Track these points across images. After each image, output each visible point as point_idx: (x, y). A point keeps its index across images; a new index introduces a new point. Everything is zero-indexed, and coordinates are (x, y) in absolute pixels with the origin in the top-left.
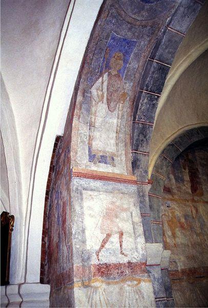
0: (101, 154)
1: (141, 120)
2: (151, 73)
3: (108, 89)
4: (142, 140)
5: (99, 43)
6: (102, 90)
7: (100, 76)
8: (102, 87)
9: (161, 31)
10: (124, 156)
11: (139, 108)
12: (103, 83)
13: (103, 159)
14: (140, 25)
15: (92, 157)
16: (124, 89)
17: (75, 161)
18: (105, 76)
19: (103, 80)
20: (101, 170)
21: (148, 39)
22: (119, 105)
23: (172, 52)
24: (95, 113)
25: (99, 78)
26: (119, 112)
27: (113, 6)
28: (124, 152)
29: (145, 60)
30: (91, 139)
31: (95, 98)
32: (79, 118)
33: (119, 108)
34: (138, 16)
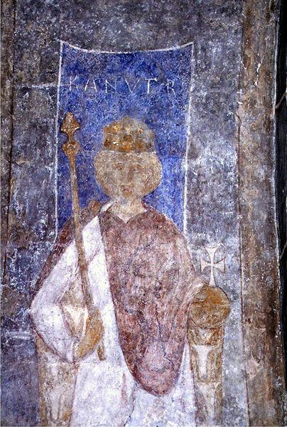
6: (87, 300)
7: (64, 240)
12: (83, 267)
16: (198, 272)
18: (91, 234)
19: (81, 253)
21: (235, 24)
22: (194, 353)
25: (60, 251)
26: (204, 388)
29: (259, 120)
31: (59, 346)
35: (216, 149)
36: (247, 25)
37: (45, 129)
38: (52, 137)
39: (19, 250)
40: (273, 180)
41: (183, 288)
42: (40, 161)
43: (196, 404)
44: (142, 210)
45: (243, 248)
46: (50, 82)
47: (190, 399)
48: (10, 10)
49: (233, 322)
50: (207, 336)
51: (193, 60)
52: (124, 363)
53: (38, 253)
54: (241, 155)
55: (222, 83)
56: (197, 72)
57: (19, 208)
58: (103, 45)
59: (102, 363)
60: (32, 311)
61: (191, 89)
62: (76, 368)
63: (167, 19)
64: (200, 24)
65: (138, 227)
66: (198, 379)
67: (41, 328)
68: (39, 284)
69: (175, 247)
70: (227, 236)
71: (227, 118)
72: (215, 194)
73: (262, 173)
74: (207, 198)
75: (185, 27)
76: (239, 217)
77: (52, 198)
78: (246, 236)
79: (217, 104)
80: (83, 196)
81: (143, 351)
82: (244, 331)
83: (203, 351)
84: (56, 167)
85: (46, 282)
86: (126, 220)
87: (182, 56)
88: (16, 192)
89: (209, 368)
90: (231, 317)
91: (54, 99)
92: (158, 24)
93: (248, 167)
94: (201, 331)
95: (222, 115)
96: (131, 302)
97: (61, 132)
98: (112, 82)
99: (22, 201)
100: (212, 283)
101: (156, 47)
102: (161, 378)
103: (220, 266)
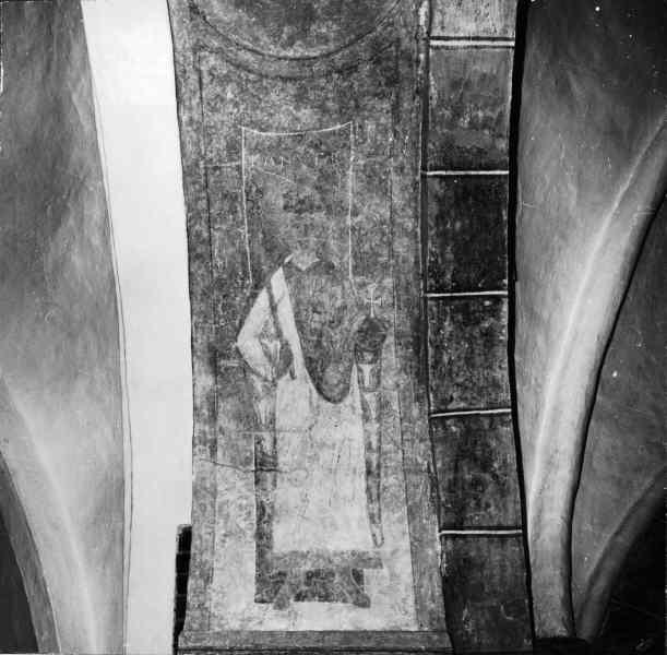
0: (308, 567)
1: (450, 407)
2: (432, 224)
3: (300, 325)
4: (477, 483)
5: (212, 180)
6: (279, 334)
7: (257, 287)
8: (276, 323)
9: (418, 61)
10: (407, 558)
11: (431, 361)
12: (273, 308)
13: (318, 585)
14: (329, 74)
15: (273, 584)
16: (362, 307)
17: (201, 606)
18: (278, 280)
19: (271, 298)
20: (304, 625)
21: (386, 105)
22: (360, 370)
23: (487, 119)
24: (273, 421)
25: (254, 296)
26: (368, 396)
27: (203, 47)
28: (405, 544)
29: (408, 181)
30: (264, 514)
31: (262, 371)
32: (213, 451)
33: (361, 381)
34: (309, 45)
35: (373, 207)
36: (396, 108)
37: (235, 198)
38: (241, 205)
39: (224, 297)
40: (419, 230)
41: (351, 320)
42: (232, 225)
43: (363, 409)
44: (317, 260)
45: (396, 287)
46: (235, 161)
47: (358, 405)
48: (198, 104)
49: (388, 346)
50: (369, 357)
51: (352, 136)
52: (309, 381)
53: (238, 299)
54: (393, 211)
55: (376, 154)
56: (356, 145)
57: (220, 263)
58: (277, 128)
59: (295, 381)
60: (239, 343)
61: (352, 159)
62: (275, 385)
63: (330, 104)
64: (357, 107)
65: (314, 274)
66: (363, 389)
67: (246, 357)
68: (241, 323)
69: (343, 288)
70: (383, 278)
71: (381, 181)
72: (373, 244)
73: (410, 225)
74: (367, 247)
75: (344, 110)
76: (392, 262)
77: (245, 253)
78: (398, 278)
79: (373, 170)
80: (269, 251)
81: (323, 371)
82: (396, 351)
83: (367, 369)
84: (246, 228)
85: (246, 321)
86: (304, 268)
87: (344, 133)
88: (216, 251)
89: (267, 436)
90: (387, 342)
91: (241, 174)
92: (324, 110)
93: (399, 220)
94: (365, 354)
95: (377, 179)
96: (312, 335)
97: (247, 200)
98: (287, 158)
99: (222, 258)
100: (372, 315)
101: (321, 128)
102: (337, 390)
103: (378, 302)
